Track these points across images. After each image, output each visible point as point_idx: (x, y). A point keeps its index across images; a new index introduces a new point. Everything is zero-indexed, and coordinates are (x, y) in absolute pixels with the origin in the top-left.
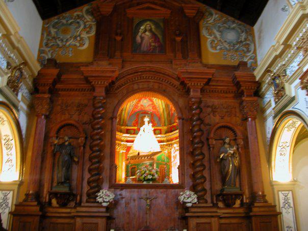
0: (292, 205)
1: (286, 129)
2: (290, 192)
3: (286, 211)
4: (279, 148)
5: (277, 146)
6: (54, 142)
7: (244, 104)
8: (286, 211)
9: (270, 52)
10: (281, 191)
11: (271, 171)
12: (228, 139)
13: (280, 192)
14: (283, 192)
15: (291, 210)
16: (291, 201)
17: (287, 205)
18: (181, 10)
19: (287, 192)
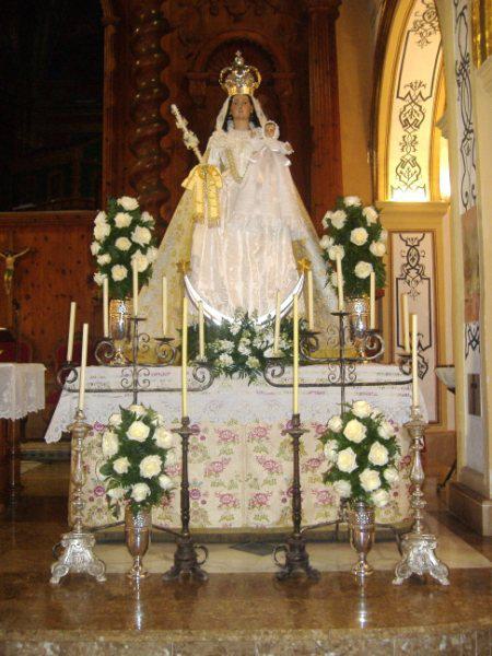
0: (429, 272)
1: (414, 38)
2: (428, 236)
3: (409, 289)
4: (398, 105)
5: (391, 97)
6: (426, 507)
7: (199, 83)
8: (409, 289)
9: (404, 43)
10: (400, 232)
11: (315, 81)
12: (383, 503)
13: (396, 237)
14: (405, 236)
15: (423, 287)
16: (427, 261)
17: (413, 273)
18: (344, 500)
19: (420, 236)
